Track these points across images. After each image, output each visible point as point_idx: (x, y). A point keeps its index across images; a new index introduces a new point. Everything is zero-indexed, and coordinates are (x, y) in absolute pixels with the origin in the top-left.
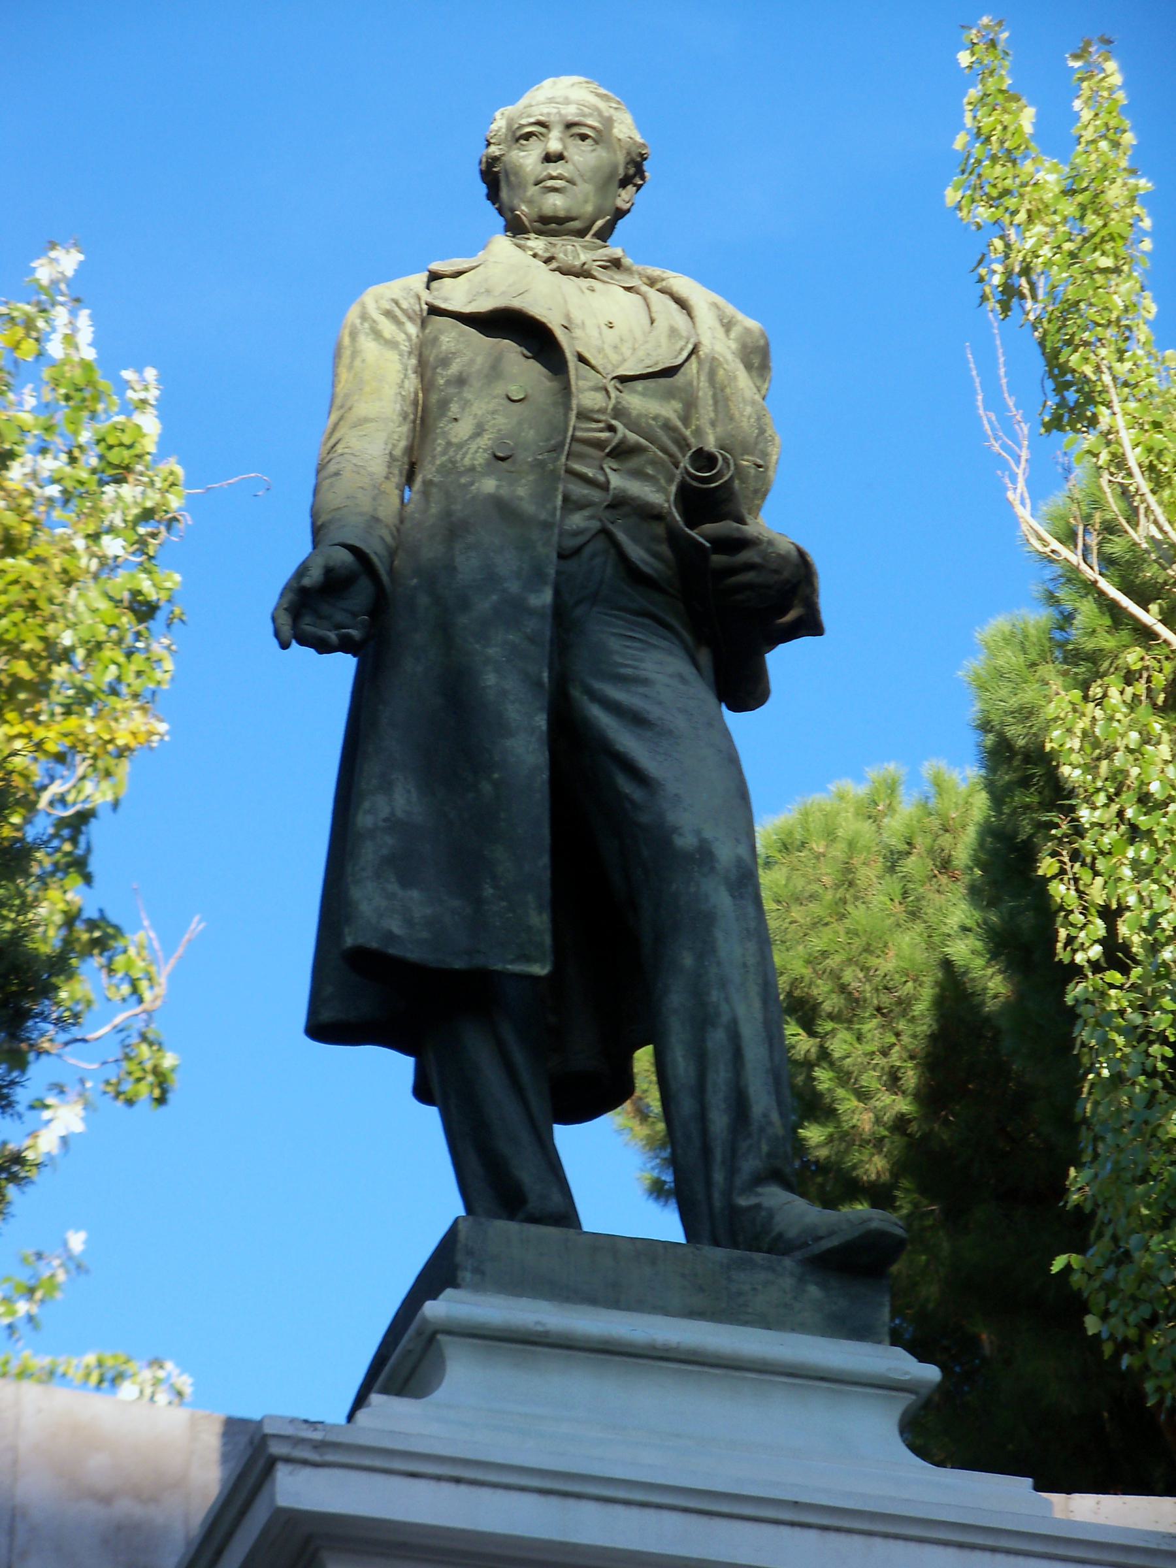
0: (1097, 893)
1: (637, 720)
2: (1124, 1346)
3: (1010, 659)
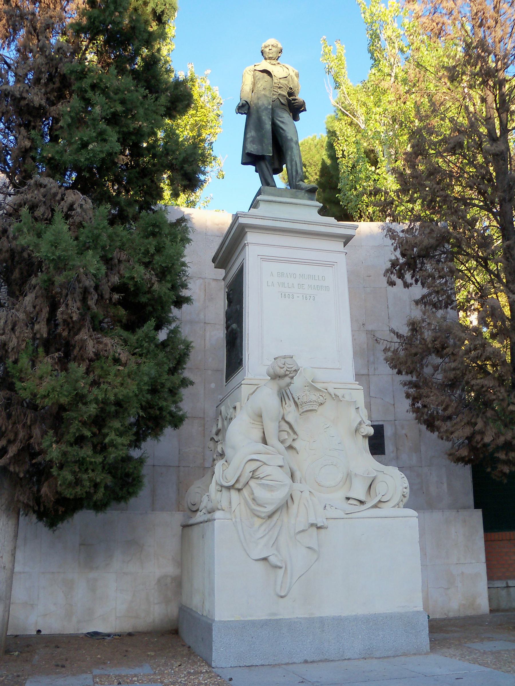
0: (341, 148)
1: (283, 122)
2: (345, 206)
3: (330, 120)
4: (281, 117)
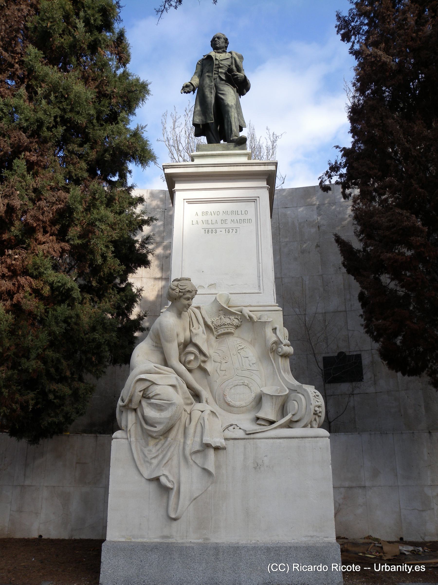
4: (222, 91)
